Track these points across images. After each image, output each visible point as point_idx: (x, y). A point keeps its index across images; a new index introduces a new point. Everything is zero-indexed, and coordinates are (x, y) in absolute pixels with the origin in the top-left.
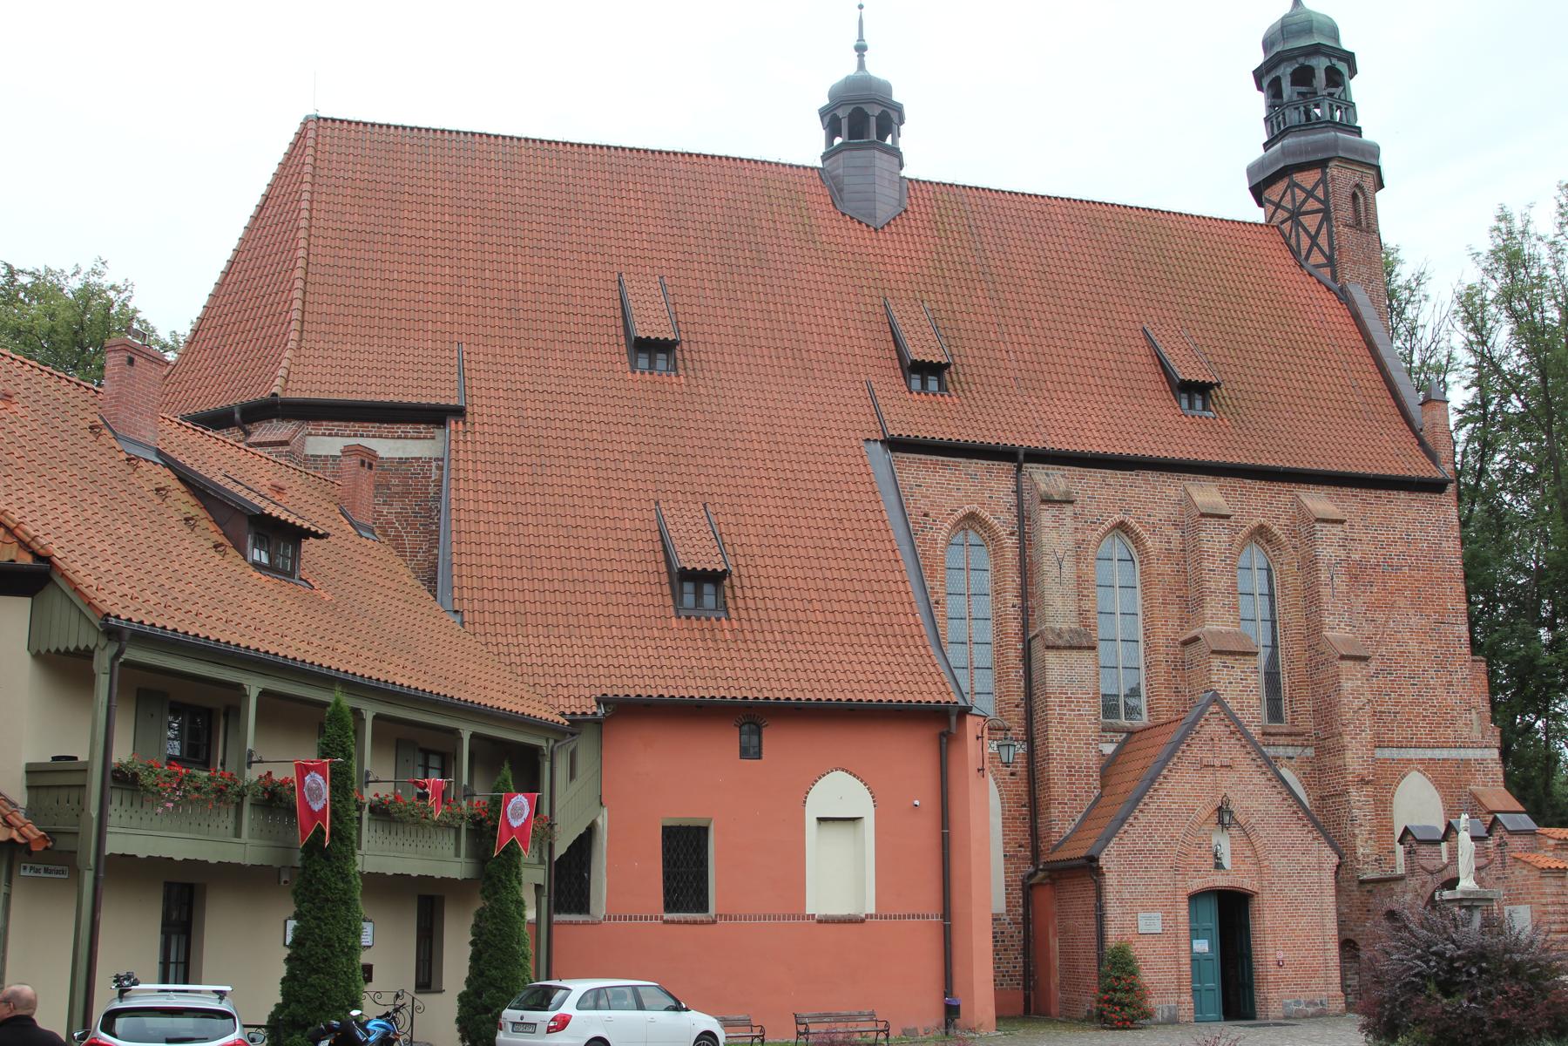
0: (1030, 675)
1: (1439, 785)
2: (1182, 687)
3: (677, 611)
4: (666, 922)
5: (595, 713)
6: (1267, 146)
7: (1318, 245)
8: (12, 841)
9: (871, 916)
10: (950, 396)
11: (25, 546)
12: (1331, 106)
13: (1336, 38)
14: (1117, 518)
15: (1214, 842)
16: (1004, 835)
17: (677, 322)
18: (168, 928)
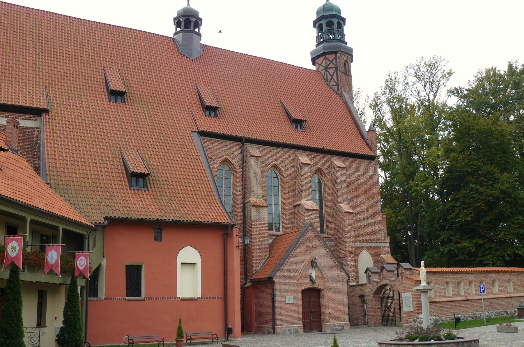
1: (372, 255)
3: (130, 187)
4: (126, 300)
5: (104, 223)
6: (317, 46)
7: (333, 79)
9: (200, 298)
10: (219, 118)
12: (338, 34)
13: (340, 13)
14: (274, 163)
15: (310, 272)
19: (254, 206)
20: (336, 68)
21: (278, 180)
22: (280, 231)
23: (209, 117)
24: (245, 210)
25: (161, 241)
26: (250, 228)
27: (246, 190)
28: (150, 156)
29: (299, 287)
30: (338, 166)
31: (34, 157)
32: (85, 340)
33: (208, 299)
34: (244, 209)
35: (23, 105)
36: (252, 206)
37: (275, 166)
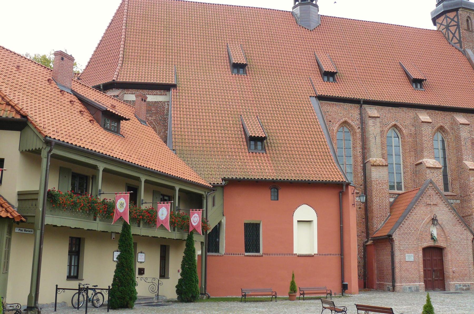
0: (365, 175)
2: (416, 180)
3: (248, 150)
4: (245, 256)
5: (221, 184)
6: (437, 5)
7: (455, 36)
8: (8, 217)
9: (316, 254)
10: (337, 83)
11: (18, 112)
14: (394, 123)
15: (431, 230)
16: (357, 228)
17: (246, 56)
18: (71, 253)
19: (373, 165)
20: (458, 26)
21: (399, 140)
22: (402, 190)
23: (327, 82)
24: (365, 170)
25: (278, 200)
26: (370, 187)
27: (366, 151)
28: (269, 121)
29: (420, 245)
30: (461, 122)
31: (165, 128)
32: (205, 291)
33: (324, 255)
34: (364, 169)
35: (154, 82)
36: (372, 165)
37: (395, 126)
